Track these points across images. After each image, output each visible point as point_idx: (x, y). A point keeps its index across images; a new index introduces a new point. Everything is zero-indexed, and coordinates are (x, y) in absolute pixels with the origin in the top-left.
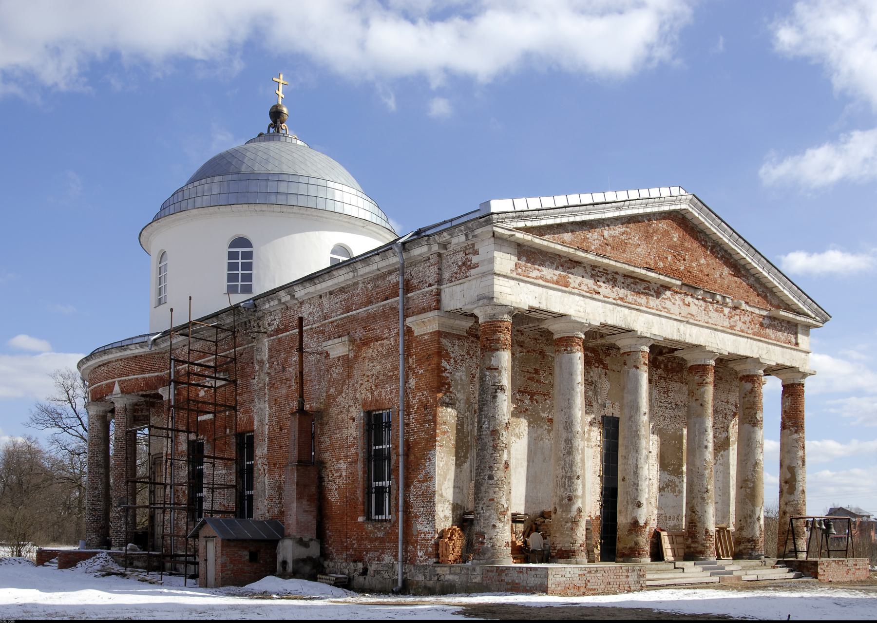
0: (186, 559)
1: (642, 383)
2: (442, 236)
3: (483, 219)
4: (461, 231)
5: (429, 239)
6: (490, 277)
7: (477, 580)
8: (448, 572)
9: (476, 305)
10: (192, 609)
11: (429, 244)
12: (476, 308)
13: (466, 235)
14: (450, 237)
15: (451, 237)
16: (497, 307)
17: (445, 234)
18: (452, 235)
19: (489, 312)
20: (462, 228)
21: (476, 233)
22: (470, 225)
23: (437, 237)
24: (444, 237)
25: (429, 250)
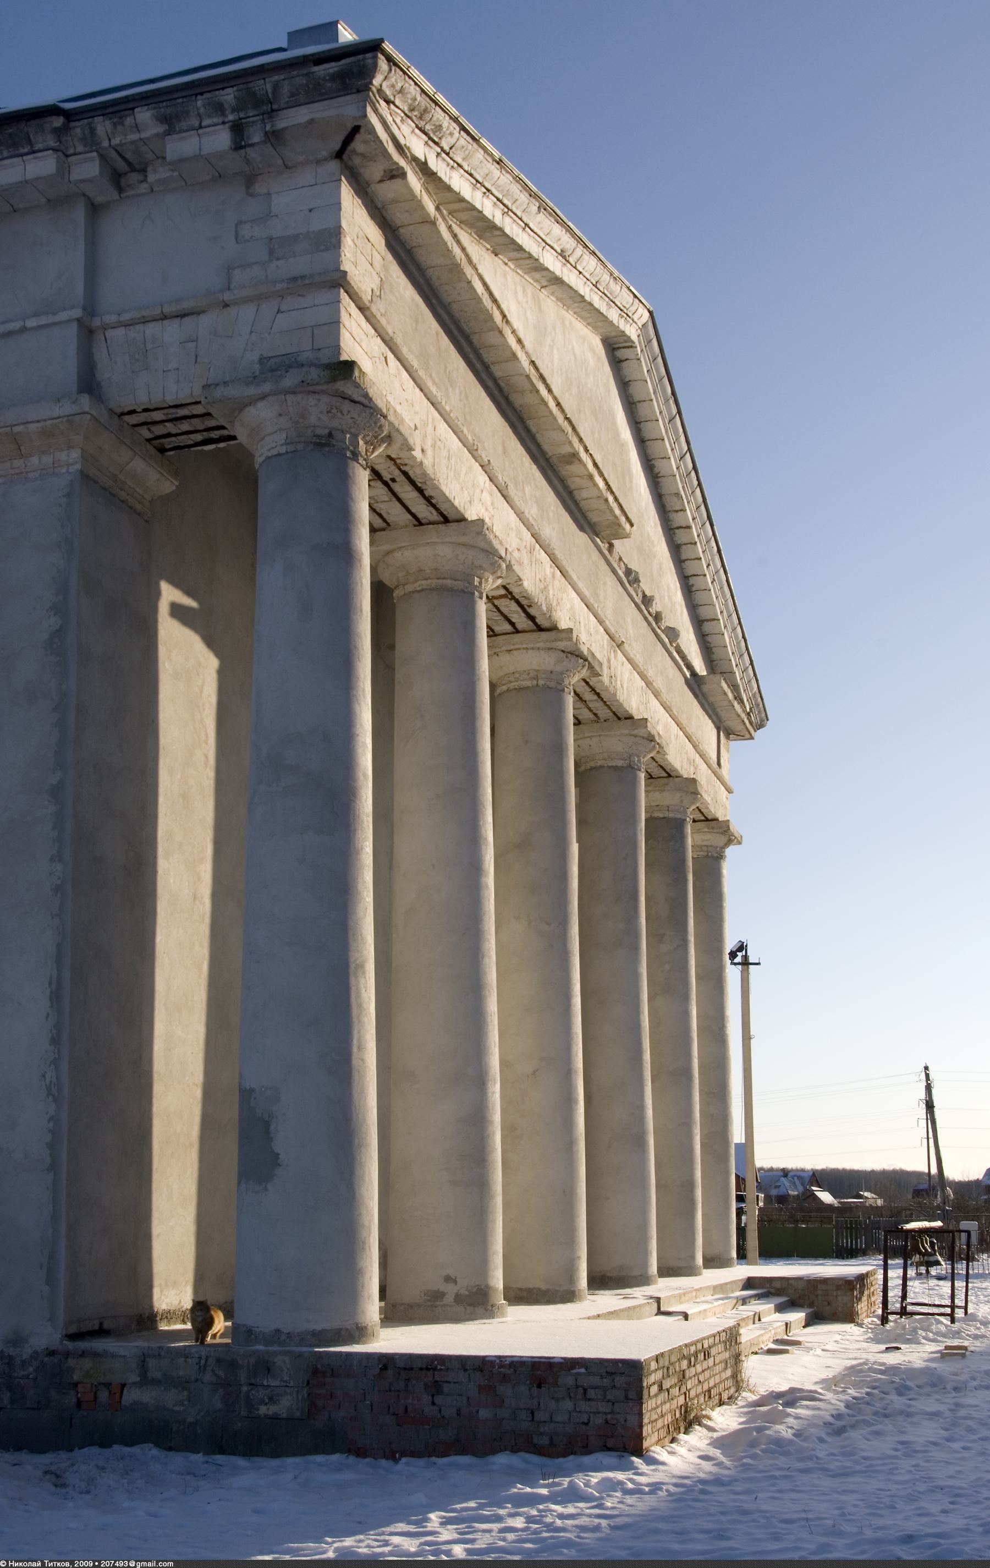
0: (959, 1307)
1: (364, 932)
2: (129, 121)
3: (332, 67)
4: (219, 108)
5: (65, 128)
6: (323, 297)
7: (285, 1406)
8: (135, 1378)
9: (267, 387)
10: (640, 881)
11: (63, 153)
12: (263, 397)
13: (238, 129)
14: (161, 129)
15: (168, 133)
16: (347, 406)
17: (144, 115)
18: (171, 123)
19: (313, 420)
20: (228, 96)
21: (281, 125)
22: (264, 86)
23: (102, 126)
24: (137, 128)
25: (63, 170)
